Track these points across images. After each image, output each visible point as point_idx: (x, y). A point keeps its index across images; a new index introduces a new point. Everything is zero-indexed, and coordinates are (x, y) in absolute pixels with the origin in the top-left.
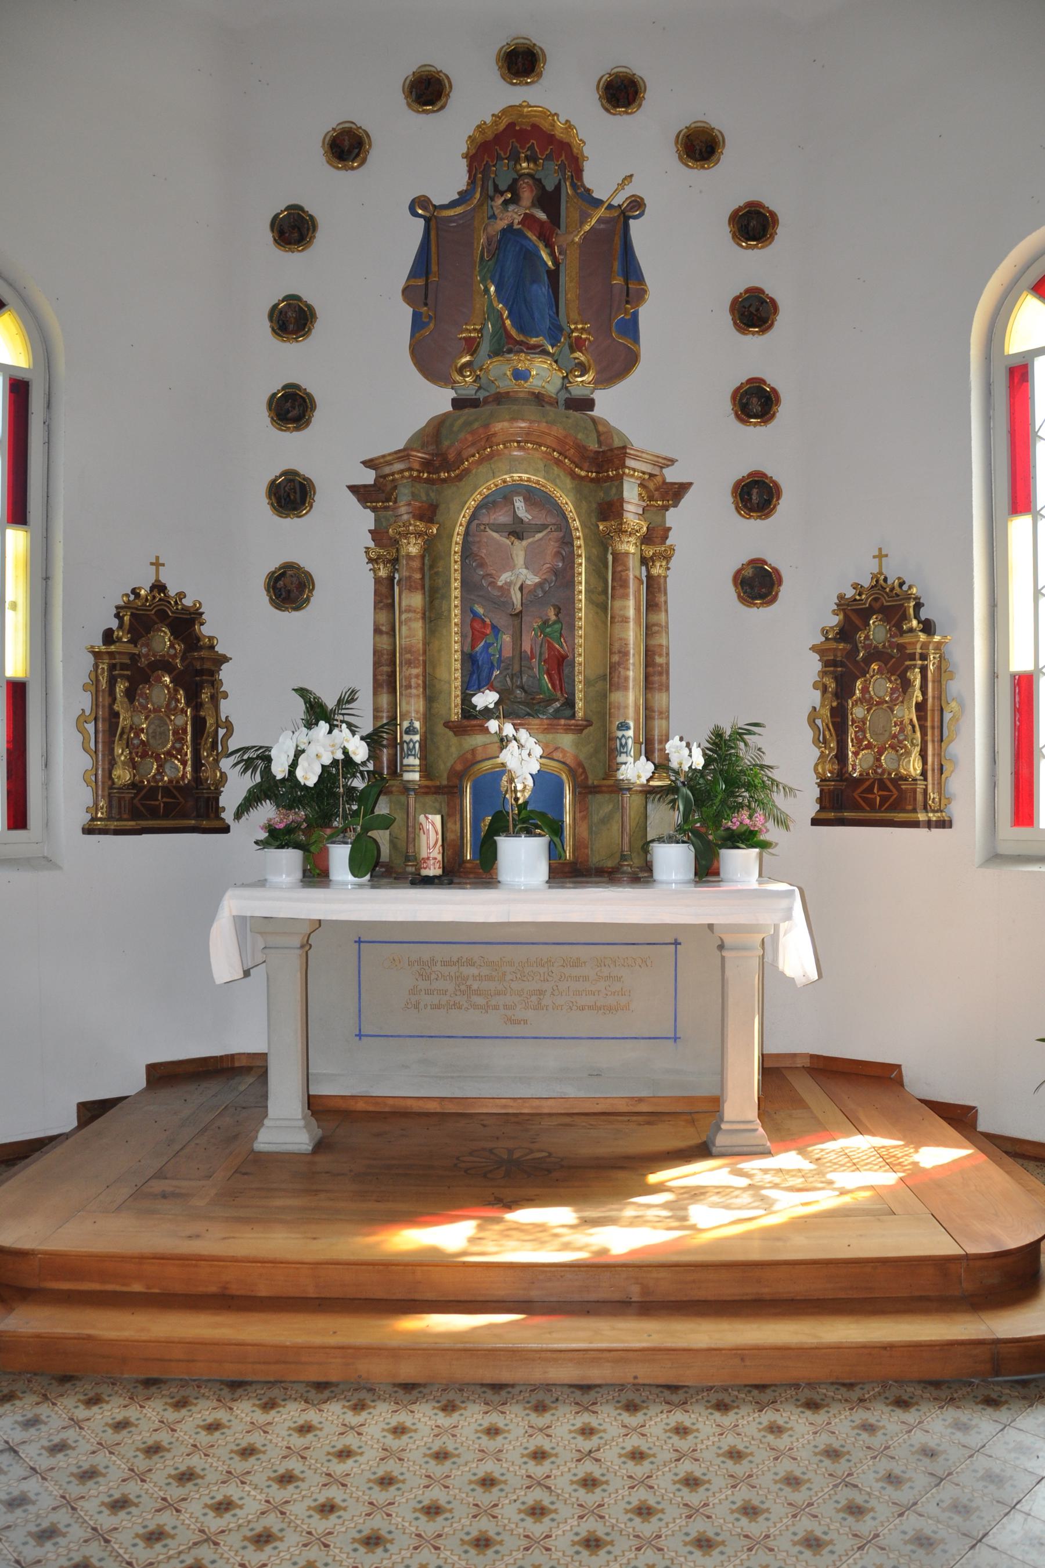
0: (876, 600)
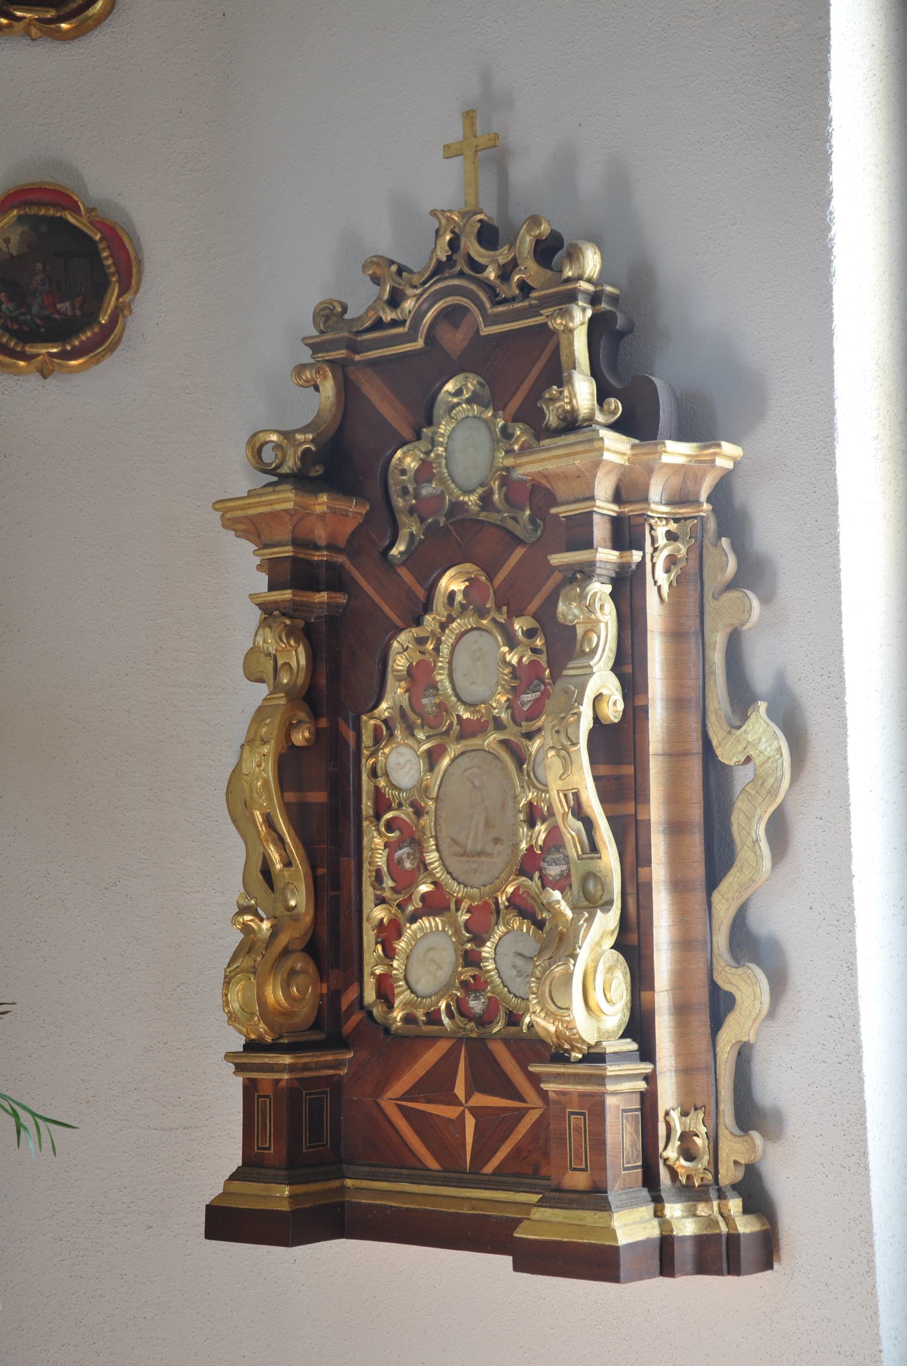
0: (453, 315)
